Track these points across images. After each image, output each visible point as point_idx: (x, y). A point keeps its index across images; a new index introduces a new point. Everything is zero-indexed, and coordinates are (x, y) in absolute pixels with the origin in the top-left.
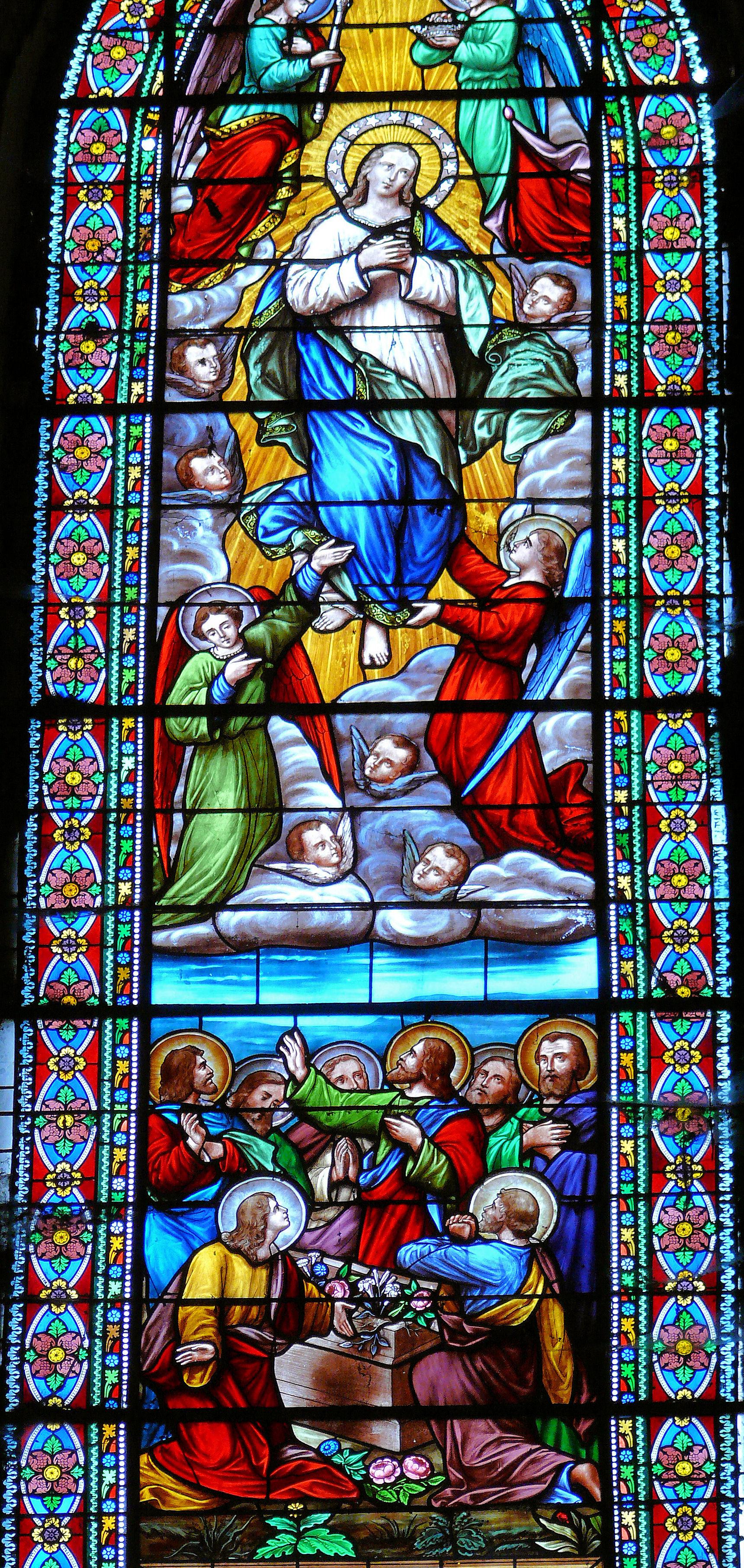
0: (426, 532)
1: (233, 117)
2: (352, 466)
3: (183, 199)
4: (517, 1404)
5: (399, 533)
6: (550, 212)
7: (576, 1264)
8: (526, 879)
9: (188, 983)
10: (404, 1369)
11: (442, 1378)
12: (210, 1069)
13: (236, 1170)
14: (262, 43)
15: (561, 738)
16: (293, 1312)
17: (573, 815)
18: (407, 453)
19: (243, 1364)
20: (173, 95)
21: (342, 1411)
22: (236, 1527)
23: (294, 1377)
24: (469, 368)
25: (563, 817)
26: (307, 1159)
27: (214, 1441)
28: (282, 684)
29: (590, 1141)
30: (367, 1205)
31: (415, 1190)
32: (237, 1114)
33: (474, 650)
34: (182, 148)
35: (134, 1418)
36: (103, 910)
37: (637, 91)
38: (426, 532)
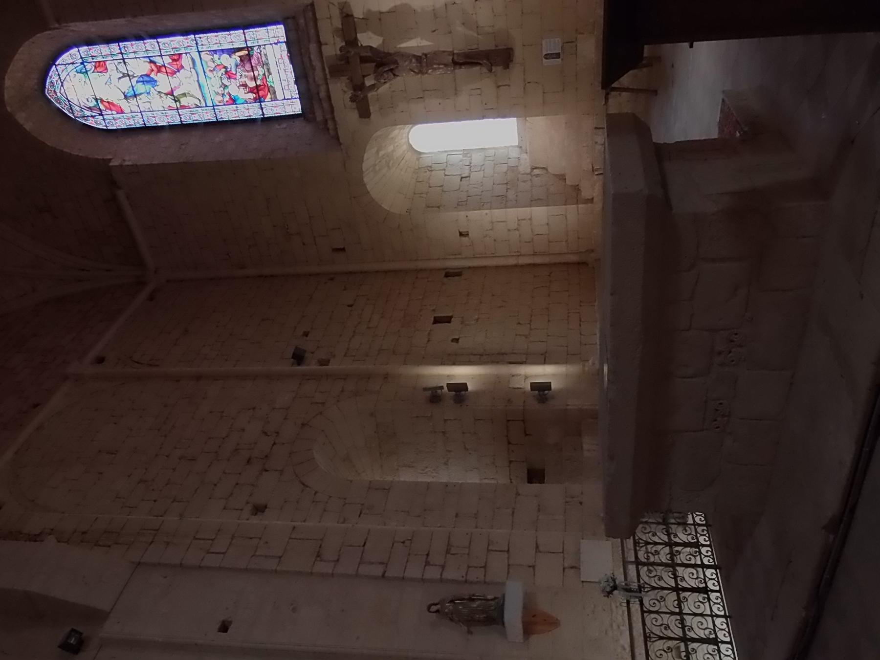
0: (146, 79)
1: (102, 107)
2: (140, 88)
3: (114, 112)
4: (249, 57)
5: (147, 82)
6: (101, 66)
7: (232, 51)
8: (185, 61)
9: (494, 148)
10: (248, 71)
11: (248, 67)
12: (220, 98)
13: (230, 95)
14: (91, 105)
15: (167, 60)
16: (245, 85)
17: (176, 57)
18: (137, 82)
19: (251, 91)
20: (101, 115)
21: (255, 78)
22: (271, 89)
23: (252, 84)
24: (124, 75)
25: (176, 58)
26: (226, 86)
27: (261, 93)
28: (171, 93)
29: (215, 51)
30: (229, 78)
31: (226, 72)
32: (223, 95)
33: (159, 71)
34: (656, 539)
35: (260, 102)
36: (199, 52)
37: (82, 58)
38: (146, 79)
